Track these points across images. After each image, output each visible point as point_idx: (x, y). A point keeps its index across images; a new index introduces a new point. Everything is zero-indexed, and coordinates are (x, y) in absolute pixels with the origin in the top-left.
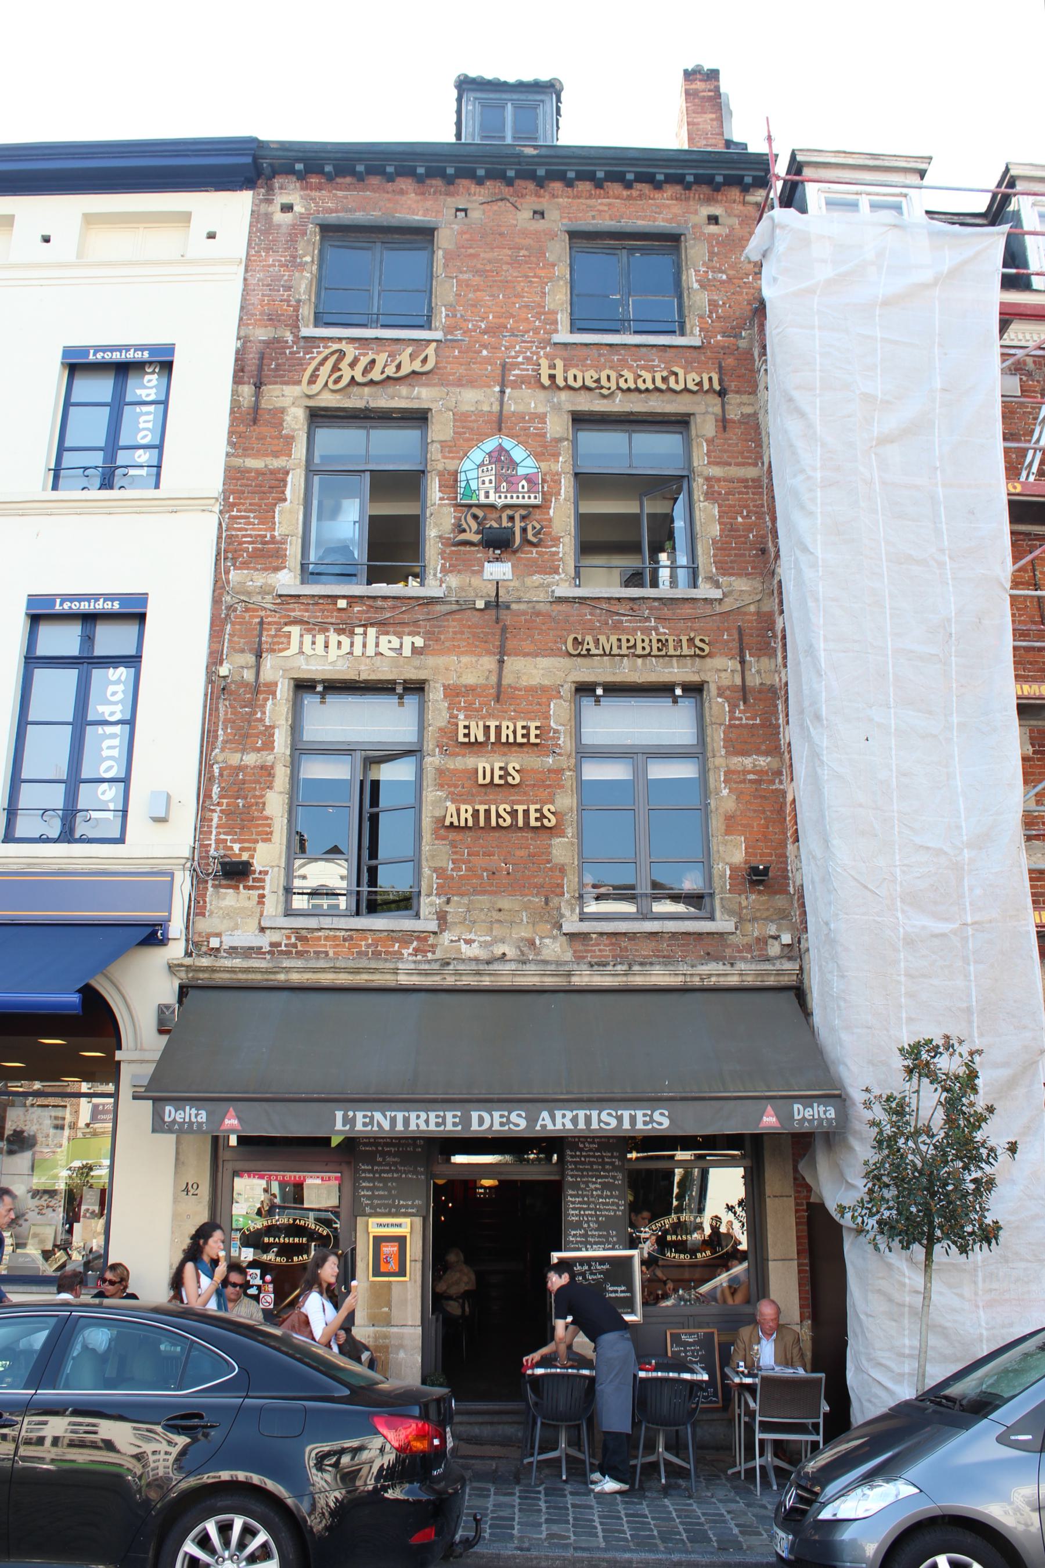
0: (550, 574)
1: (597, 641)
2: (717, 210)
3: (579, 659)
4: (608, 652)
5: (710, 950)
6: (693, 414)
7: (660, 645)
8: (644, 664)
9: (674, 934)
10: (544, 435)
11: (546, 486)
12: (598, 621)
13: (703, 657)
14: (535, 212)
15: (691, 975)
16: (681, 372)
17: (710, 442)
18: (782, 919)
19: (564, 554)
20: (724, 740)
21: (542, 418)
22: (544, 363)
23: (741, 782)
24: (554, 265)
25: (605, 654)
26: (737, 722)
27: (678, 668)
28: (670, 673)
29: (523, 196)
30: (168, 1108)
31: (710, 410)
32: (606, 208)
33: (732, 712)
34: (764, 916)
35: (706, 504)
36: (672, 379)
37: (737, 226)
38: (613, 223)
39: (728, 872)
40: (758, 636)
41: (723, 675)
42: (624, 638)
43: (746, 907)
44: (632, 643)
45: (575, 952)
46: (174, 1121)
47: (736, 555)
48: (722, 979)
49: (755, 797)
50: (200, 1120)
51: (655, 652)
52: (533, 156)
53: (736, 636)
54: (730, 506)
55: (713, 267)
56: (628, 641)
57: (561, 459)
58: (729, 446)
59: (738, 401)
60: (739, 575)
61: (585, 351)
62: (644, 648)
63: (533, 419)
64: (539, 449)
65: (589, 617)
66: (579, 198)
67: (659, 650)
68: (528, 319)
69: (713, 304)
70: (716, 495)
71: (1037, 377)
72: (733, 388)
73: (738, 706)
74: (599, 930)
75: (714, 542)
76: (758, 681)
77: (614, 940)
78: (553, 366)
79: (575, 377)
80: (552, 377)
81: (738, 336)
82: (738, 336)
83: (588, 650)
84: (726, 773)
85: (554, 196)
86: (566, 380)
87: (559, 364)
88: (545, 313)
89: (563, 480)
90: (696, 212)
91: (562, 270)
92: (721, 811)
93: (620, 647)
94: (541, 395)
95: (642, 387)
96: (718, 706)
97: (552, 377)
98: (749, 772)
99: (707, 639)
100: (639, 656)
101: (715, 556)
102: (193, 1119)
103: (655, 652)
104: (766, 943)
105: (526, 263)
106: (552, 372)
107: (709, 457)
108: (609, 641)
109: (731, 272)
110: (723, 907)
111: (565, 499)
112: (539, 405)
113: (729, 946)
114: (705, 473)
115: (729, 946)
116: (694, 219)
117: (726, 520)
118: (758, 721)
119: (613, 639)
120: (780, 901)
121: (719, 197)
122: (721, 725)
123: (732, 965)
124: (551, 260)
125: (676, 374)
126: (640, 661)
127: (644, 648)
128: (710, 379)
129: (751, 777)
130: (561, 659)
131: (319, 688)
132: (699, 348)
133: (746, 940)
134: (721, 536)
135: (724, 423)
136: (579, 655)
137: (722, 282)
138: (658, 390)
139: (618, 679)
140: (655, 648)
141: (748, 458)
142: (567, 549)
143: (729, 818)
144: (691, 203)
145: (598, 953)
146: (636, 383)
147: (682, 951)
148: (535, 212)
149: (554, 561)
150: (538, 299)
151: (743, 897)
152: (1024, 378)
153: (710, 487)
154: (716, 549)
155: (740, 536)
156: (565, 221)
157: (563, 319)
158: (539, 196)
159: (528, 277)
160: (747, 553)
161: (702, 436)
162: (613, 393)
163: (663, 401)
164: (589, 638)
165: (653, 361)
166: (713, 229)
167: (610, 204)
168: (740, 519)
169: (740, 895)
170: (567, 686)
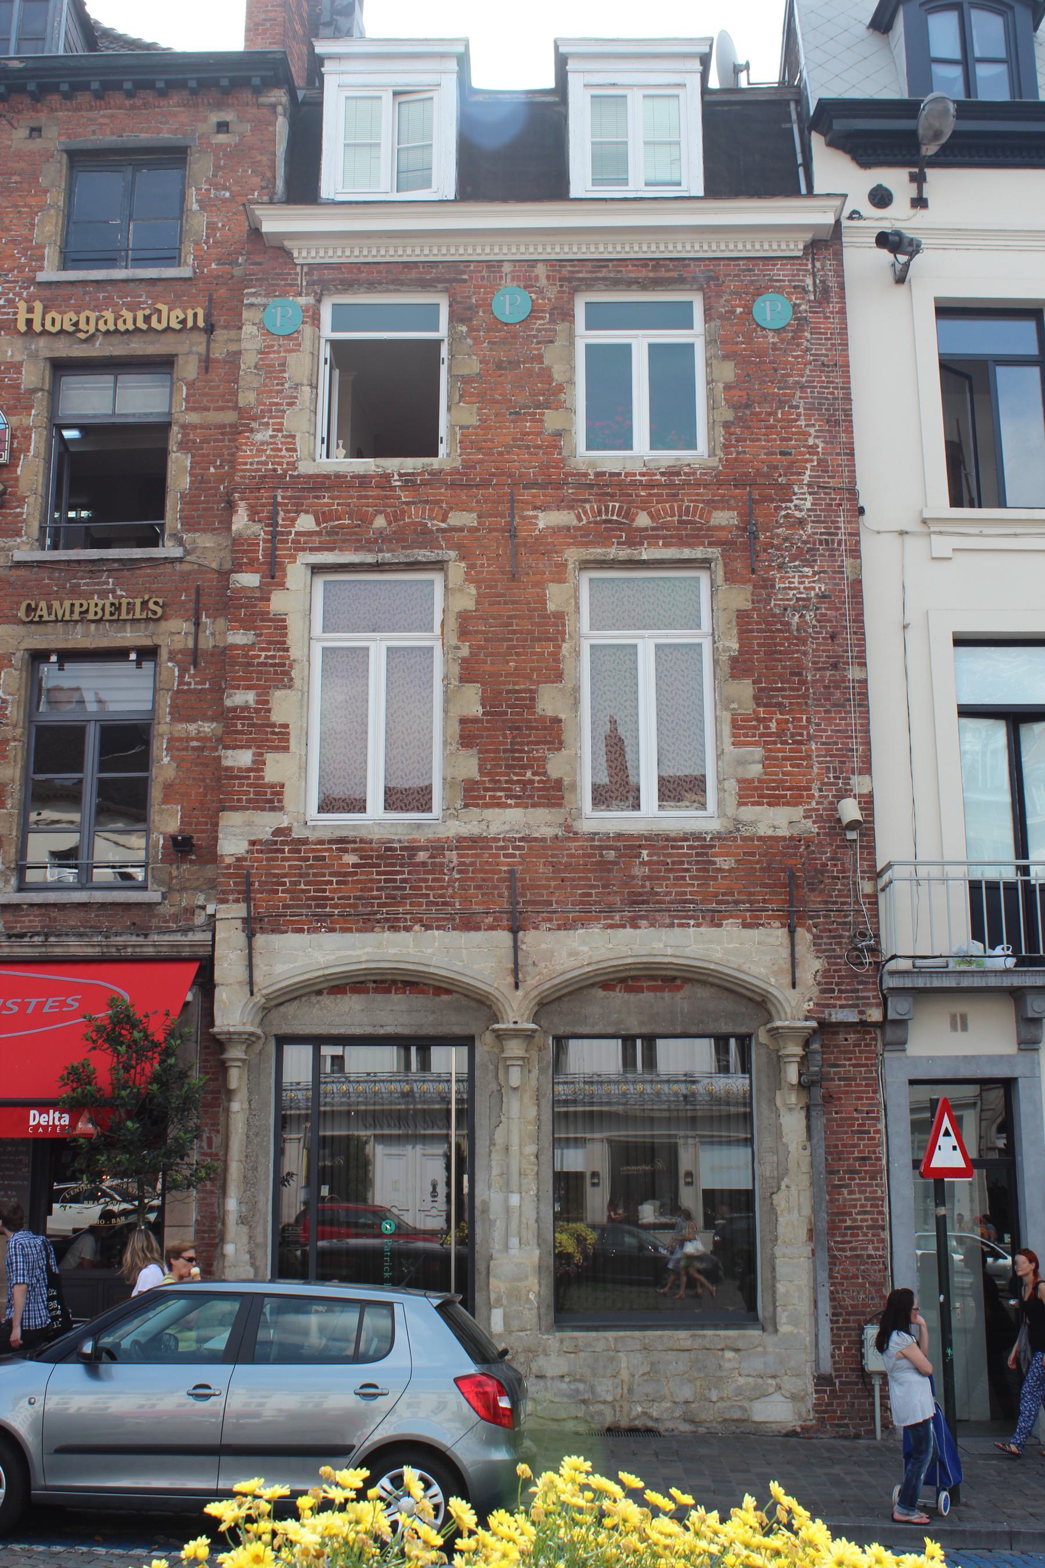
0: (12, 536)
1: (50, 608)
2: (229, 116)
3: (33, 627)
4: (60, 618)
5: (137, 920)
6: (177, 355)
7: (113, 609)
8: (97, 629)
9: (103, 905)
10: (18, 387)
11: (15, 442)
12: (56, 585)
13: (158, 620)
14: (33, 130)
15: (107, 946)
16: (164, 308)
17: (190, 385)
18: (212, 888)
19: (28, 515)
20: (171, 706)
21: (17, 367)
22: (22, 306)
23: (183, 749)
24: (46, 191)
25: (56, 621)
26: (186, 687)
27: (131, 632)
28: (122, 637)
29: (20, 112)
30: (32, 1112)
31: (194, 349)
32: (107, 121)
33: (181, 676)
34: (194, 886)
35: (179, 454)
36: (154, 318)
37: (249, 133)
38: (114, 138)
39: (161, 842)
40: (216, 596)
41: (177, 638)
42: (77, 603)
43: (176, 877)
44: (84, 608)
45: (6, 922)
46: (39, 1125)
47: (204, 509)
48: (138, 950)
49: (197, 765)
50: (63, 1123)
51: (107, 617)
52: (20, 70)
53: (193, 597)
54: (203, 455)
55: (216, 184)
56: (81, 605)
57: (33, 412)
58: (211, 388)
59: (225, 337)
60: (204, 531)
61: (69, 290)
62: (96, 613)
63: (9, 369)
64: (12, 402)
65: (47, 581)
66: (80, 110)
67: (112, 614)
68: (13, 255)
69: (211, 227)
70: (190, 444)
71: (549, 295)
72: (222, 323)
73: (188, 670)
74: (28, 901)
75: (183, 495)
76: (211, 644)
77: (43, 911)
78: (30, 310)
79: (53, 320)
80: (29, 322)
81: (234, 263)
82: (234, 263)
83: (41, 616)
84: (169, 741)
85: (52, 110)
86: (43, 325)
87: (38, 306)
88: (32, 248)
89: (33, 435)
90: (205, 120)
91: (56, 197)
92: (161, 779)
93: (72, 612)
94: (19, 342)
95: (122, 327)
96: (170, 668)
97: (29, 322)
98: (193, 739)
99: (160, 601)
100: (93, 621)
101: (181, 511)
102: (57, 1123)
103: (107, 617)
104: (193, 913)
105: (18, 190)
106: (30, 316)
107: (187, 402)
108: (63, 608)
109: (235, 189)
110: (153, 877)
111: (34, 456)
112: (16, 353)
113: (156, 916)
114: (181, 420)
115: (156, 916)
116: (202, 128)
117: (198, 471)
118: (207, 686)
119: (67, 604)
120: (209, 871)
121: (230, 101)
122: (168, 690)
123: (146, 936)
124: (43, 185)
125: (160, 311)
126: (93, 626)
127: (96, 613)
128: (195, 315)
129: (195, 744)
130: (15, 627)
131: (133, 656)
132: (190, 279)
133: (173, 910)
134: (190, 489)
135: (207, 363)
136: (31, 622)
137: (224, 201)
138: (137, 330)
139: (70, 645)
140: (107, 612)
141: (228, 401)
142: (31, 510)
143: (168, 787)
144: (201, 109)
145: (27, 924)
146: (116, 325)
147: (109, 921)
148: (33, 130)
149: (17, 522)
150: (26, 232)
151: (174, 866)
152: (534, 296)
153: (185, 435)
154: (184, 503)
155: (210, 489)
156: (63, 139)
157: (51, 254)
158: (37, 111)
159: (17, 206)
160: (215, 506)
161: (182, 380)
162: (93, 335)
163: (145, 342)
164: (43, 604)
165: (140, 296)
166: (222, 138)
167: (112, 116)
168: (212, 470)
169: (171, 865)
170: (19, 654)
